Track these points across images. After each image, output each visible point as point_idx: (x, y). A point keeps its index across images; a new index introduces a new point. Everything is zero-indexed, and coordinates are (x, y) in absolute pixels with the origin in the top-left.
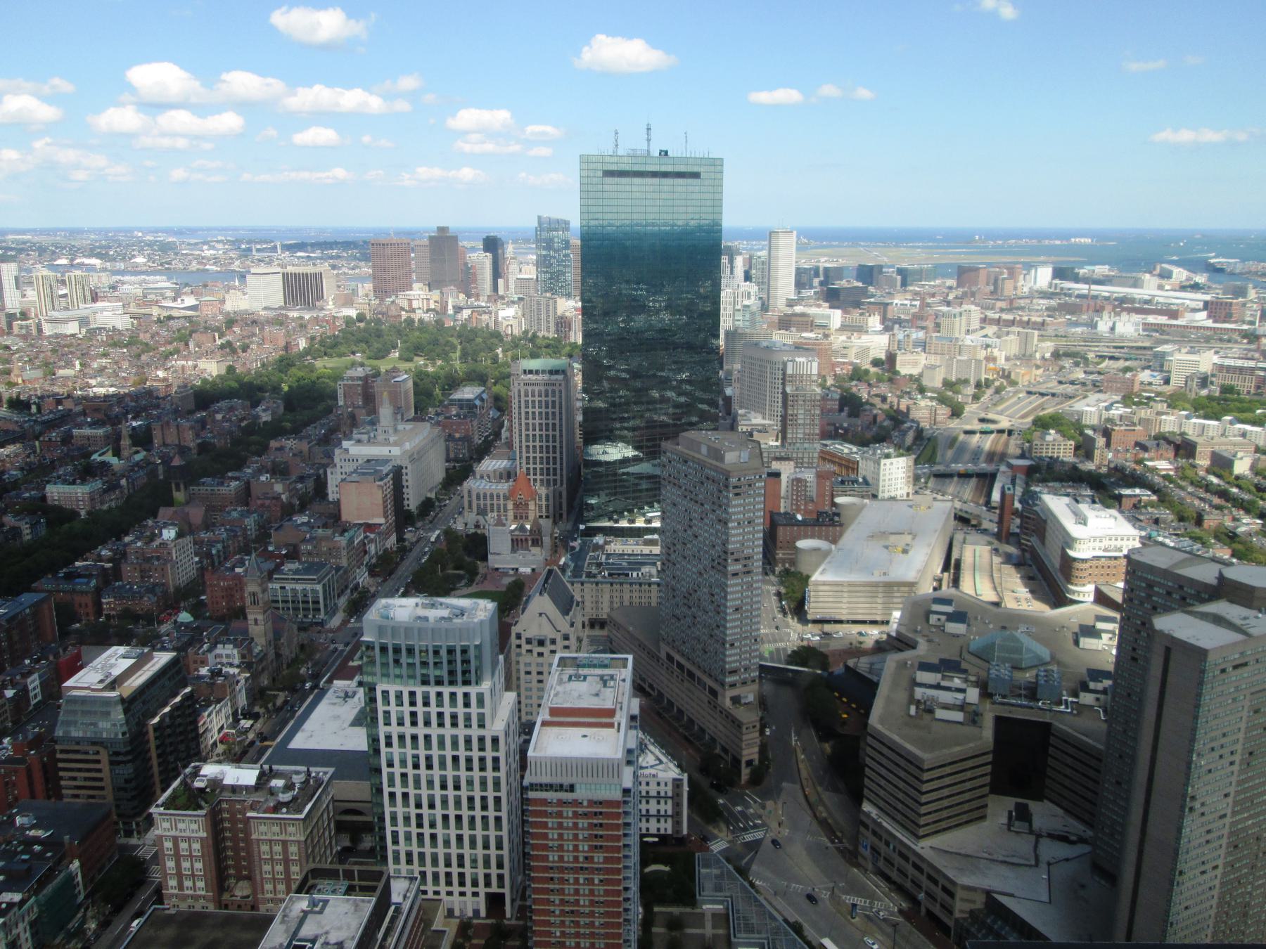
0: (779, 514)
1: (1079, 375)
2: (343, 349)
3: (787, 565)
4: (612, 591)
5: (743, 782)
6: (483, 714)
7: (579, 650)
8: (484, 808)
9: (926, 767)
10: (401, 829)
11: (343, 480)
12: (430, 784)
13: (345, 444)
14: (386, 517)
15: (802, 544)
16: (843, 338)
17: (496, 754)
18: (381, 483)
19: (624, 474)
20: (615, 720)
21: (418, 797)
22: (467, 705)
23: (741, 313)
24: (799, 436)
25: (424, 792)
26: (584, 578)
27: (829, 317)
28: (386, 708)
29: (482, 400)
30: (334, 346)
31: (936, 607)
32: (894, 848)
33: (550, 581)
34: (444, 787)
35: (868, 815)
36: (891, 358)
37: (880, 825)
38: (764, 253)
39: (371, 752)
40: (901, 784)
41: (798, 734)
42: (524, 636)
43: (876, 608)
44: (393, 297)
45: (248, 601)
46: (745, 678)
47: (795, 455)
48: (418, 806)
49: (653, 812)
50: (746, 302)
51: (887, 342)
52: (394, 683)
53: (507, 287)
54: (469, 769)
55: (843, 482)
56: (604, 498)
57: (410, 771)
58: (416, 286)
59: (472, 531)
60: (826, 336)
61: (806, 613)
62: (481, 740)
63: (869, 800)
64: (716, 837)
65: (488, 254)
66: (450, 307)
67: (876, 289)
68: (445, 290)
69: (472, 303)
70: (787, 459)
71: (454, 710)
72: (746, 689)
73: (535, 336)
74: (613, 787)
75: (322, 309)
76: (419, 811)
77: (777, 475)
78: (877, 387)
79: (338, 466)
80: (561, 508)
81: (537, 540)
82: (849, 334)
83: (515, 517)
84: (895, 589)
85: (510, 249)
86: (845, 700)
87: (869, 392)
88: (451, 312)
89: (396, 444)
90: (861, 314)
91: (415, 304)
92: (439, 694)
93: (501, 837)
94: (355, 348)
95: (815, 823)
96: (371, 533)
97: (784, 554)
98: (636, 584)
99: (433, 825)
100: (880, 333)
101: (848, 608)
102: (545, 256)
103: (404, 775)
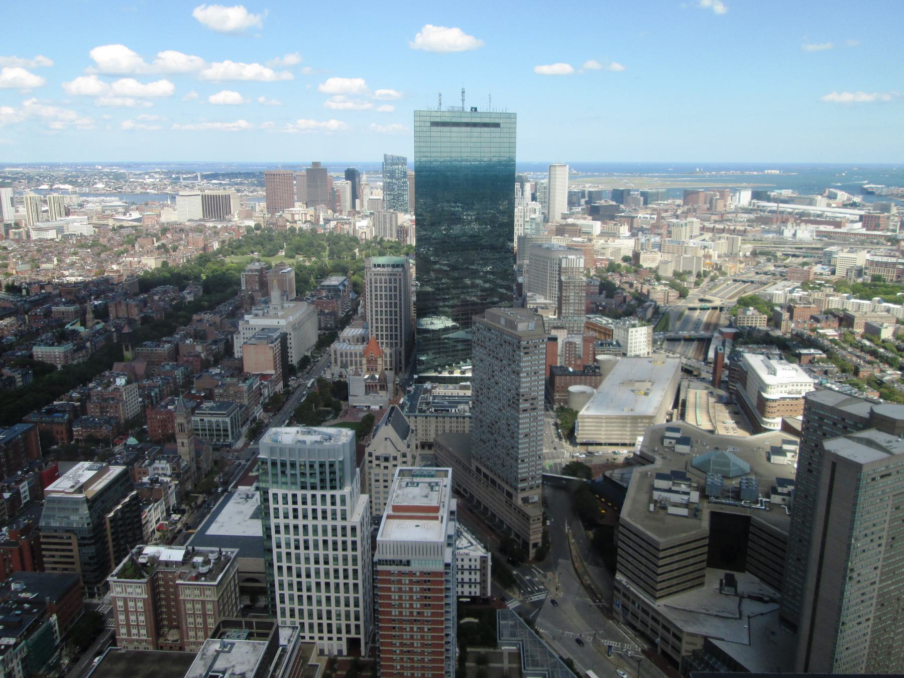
0: (557, 367)
1: (771, 268)
2: (245, 249)
3: (562, 404)
4: (437, 422)
5: (530, 559)
6: (345, 510)
7: (413, 464)
8: (346, 577)
9: (661, 548)
10: (286, 592)
11: (245, 343)
12: (307, 560)
13: (247, 317)
14: (276, 370)
15: (573, 389)
16: (602, 241)
17: (354, 539)
18: (272, 345)
19: (445, 338)
20: (439, 514)
21: (299, 570)
22: (333, 503)
23: (529, 223)
24: (571, 311)
25: (303, 566)
26: (417, 413)
27: (592, 226)
28: (276, 506)
29: (344, 286)
30: (239, 247)
31: (668, 434)
32: (639, 606)
33: (393, 415)
34: (317, 562)
35: (620, 582)
36: (636, 256)
37: (628, 589)
38: (545, 181)
39: (265, 537)
40: (644, 560)
41: (570, 524)
42: (374, 454)
43: (625, 435)
44: (281, 212)
45: (177, 429)
46: (532, 485)
47: (567, 325)
48: (299, 576)
49: (466, 580)
50: (533, 216)
51: (633, 244)
52: (282, 488)
53: (362, 205)
54: (335, 549)
55: (602, 345)
56: (431, 356)
57: (293, 551)
58: (297, 204)
59: (337, 379)
60: (590, 240)
61: (575, 438)
62: (344, 528)
63: (620, 571)
64: (511, 598)
65: (348, 182)
66: (321, 219)
67: (626, 206)
68: (317, 207)
69: (337, 216)
70: (562, 328)
71: (324, 507)
72: (533, 492)
73: (382, 240)
74: (438, 562)
75: (230, 221)
76: (299, 580)
77: (555, 339)
78: (626, 276)
79: (242, 333)
80: (400, 363)
81: (384, 386)
82: (607, 239)
83: (368, 370)
84: (639, 420)
85: (364, 178)
86: (603, 500)
87: (621, 280)
88: (322, 223)
89: (283, 317)
90: (615, 225)
91: (297, 217)
92: (314, 496)
93: (358, 598)
94: (253, 249)
95: (582, 588)
96: (265, 381)
97: (560, 396)
98: (454, 417)
99: (309, 589)
100: (629, 238)
101: (606, 434)
102: (389, 183)
103: (288, 554)
